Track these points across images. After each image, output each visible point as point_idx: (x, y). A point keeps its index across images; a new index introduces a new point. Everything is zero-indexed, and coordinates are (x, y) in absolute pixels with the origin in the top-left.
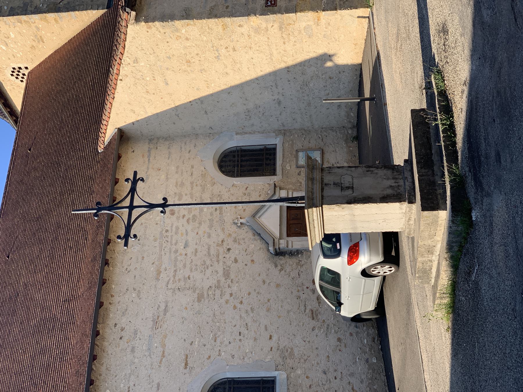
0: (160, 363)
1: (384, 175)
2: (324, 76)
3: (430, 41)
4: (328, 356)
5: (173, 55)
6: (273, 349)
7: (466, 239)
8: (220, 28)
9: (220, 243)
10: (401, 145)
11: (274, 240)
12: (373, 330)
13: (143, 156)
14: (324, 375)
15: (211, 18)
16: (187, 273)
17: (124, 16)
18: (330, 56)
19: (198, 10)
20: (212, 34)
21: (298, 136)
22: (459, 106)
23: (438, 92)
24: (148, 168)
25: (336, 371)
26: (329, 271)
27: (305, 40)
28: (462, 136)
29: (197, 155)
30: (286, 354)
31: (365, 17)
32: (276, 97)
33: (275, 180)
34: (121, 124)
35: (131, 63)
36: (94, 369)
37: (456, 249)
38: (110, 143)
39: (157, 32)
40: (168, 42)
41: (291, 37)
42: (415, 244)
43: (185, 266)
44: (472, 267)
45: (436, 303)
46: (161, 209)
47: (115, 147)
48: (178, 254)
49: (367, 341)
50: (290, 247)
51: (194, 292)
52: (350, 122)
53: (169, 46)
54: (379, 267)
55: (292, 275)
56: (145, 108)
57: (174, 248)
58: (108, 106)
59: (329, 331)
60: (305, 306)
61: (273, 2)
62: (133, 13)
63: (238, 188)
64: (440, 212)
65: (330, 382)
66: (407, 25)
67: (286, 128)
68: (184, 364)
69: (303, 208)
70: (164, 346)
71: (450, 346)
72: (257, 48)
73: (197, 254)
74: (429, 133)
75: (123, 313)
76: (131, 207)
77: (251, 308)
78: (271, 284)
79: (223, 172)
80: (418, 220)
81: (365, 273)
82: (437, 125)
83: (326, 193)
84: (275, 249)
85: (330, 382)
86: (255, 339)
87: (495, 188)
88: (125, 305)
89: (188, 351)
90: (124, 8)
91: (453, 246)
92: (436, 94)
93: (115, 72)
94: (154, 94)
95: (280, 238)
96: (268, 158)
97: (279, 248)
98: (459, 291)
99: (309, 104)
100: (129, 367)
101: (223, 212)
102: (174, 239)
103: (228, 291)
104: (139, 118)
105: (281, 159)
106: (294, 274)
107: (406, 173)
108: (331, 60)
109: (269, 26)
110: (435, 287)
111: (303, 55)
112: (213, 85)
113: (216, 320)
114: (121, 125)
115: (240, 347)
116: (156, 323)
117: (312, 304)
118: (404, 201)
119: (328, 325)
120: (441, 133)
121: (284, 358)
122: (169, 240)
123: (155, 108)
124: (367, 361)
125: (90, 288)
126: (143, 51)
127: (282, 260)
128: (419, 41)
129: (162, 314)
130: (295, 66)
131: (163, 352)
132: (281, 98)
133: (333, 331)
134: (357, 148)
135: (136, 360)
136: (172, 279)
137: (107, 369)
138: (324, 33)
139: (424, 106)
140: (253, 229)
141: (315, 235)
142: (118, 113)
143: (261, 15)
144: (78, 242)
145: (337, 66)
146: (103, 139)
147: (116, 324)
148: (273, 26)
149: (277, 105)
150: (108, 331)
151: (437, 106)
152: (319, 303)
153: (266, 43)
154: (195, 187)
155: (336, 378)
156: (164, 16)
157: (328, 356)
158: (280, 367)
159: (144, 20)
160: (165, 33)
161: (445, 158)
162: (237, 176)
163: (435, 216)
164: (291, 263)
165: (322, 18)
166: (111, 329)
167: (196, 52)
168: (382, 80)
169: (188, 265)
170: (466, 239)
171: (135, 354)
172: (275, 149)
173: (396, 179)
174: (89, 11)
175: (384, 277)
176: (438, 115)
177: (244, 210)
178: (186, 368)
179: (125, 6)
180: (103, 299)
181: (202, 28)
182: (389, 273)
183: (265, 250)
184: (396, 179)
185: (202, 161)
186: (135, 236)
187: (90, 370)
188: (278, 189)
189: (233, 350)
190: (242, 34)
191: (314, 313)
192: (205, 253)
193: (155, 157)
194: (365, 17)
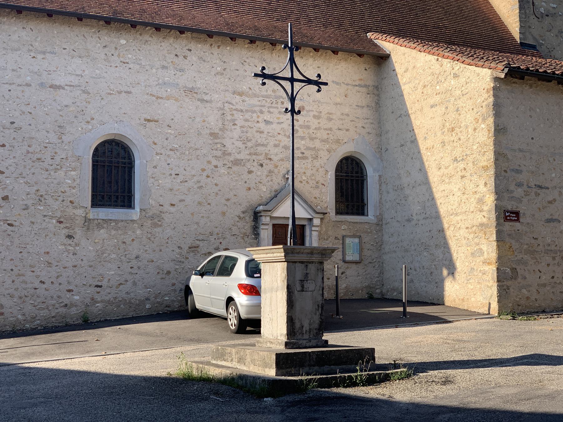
0: (151, 94)
1: (313, 321)
2: (433, 267)
3: (442, 369)
4: (153, 261)
5: (460, 114)
6: (161, 207)
7: (248, 391)
8: (485, 164)
9: (269, 157)
10: (352, 340)
11: (270, 211)
12: (177, 306)
13: (361, 80)
14: (135, 256)
15: (495, 155)
16: (240, 123)
17: (501, 66)
18: (453, 273)
19: (504, 142)
20: (479, 155)
21: (375, 238)
22: (372, 392)
23: (389, 373)
24: (347, 84)
25: (139, 268)
26: (234, 265)
27: (469, 249)
28: (342, 392)
29: (360, 134)
30: (156, 219)
31: (489, 310)
32: (415, 217)
33: (331, 214)
34: (394, 58)
35: (454, 71)
36: (147, 29)
37: (240, 383)
38: (376, 45)
39: (483, 99)
40: (473, 109)
41: (473, 235)
42: (247, 347)
43: (246, 120)
44: (222, 396)
45: (194, 364)
46: (289, 109)
47: (371, 51)
48: (259, 114)
49: (167, 300)
50: (262, 227)
51: (220, 130)
52: (388, 291)
53: (469, 110)
54: (236, 314)
55: (234, 228)
56: (409, 83)
57: (265, 110)
58: (412, 45)
59: (177, 263)
60: (203, 240)
61: (508, 218)
62: (503, 76)
63: (324, 176)
64: (275, 370)
65: (128, 262)
66: (466, 349)
67: (384, 226)
68: (149, 118)
69: (285, 243)
70: (168, 98)
71: (154, 375)
72: (463, 201)
73: (258, 134)
74: (352, 364)
75: (201, 58)
76: (292, 80)
77: (202, 186)
78: (226, 207)
79: (341, 161)
80: (269, 350)
81: (230, 300)
82: (356, 371)
83: (299, 267)
84: (260, 212)
85: (128, 262)
86: (171, 190)
87: (287, 416)
88: (209, 59)
89: (162, 122)
90: (508, 66)
91: (242, 380)
92: (387, 372)
93: (446, 54)
94: (423, 93)
95: (272, 218)
96: (354, 207)
97: (261, 216)
98: (202, 385)
99: (406, 251)
100: (148, 63)
101: (300, 160)
102: (275, 110)
103: (220, 164)
104: (399, 76)
105: (352, 221)
106: (235, 230)
107: (315, 341)
108: (449, 274)
109: (484, 213)
110: (209, 363)
111: (455, 246)
112: (429, 154)
113: (191, 151)
114: (394, 57)
115: (164, 174)
116: (191, 91)
117: (204, 247)
118: (288, 339)
119: (183, 262)
120: (349, 374)
121: (152, 218)
122: (273, 105)
123: (409, 93)
124: (147, 299)
125: (228, 24)
126: (465, 83)
127: (249, 218)
128: (445, 360)
129: (199, 96)
130: (445, 238)
131: (162, 98)
132: (413, 223)
133: (178, 267)
134: (361, 297)
135: (154, 70)
136: (234, 107)
137: (147, 41)
138: (475, 268)
139: (378, 362)
140: (282, 189)
141: (260, 254)
142: (406, 55)
143: (496, 205)
144: (275, 11)
145: (442, 281)
146: (380, 38)
147: (190, 50)
148: (485, 217)
149: (406, 218)
150: (184, 42)
151: (375, 372)
152: (205, 254)
153: (468, 210)
154: (327, 132)
155: (131, 268)
156: (499, 107)
157: (153, 261)
158: (144, 213)
159: (496, 86)
160: (482, 107)
161: (325, 376)
162: (336, 176)
163: (271, 365)
164: (246, 228)
165: (490, 267)
166: (186, 46)
167: (462, 138)
168: (422, 325)
169: (247, 124)
170: (248, 391)
171: (160, 70)
172: (363, 214)
173: (310, 332)
174: (518, 24)
175: (226, 319)
176: (366, 373)
177: (301, 182)
178: (145, 120)
179: (510, 68)
180: (215, 38)
181: (486, 145)
182: (230, 323)
183: (260, 202)
184: (310, 332)
185: (353, 140)
186: (264, 84)
187: (146, 24)
188: (321, 216)
189: (161, 167)
190: (477, 186)
191: (195, 249)
192: (259, 141)
193: (359, 92)
194: (489, 310)
